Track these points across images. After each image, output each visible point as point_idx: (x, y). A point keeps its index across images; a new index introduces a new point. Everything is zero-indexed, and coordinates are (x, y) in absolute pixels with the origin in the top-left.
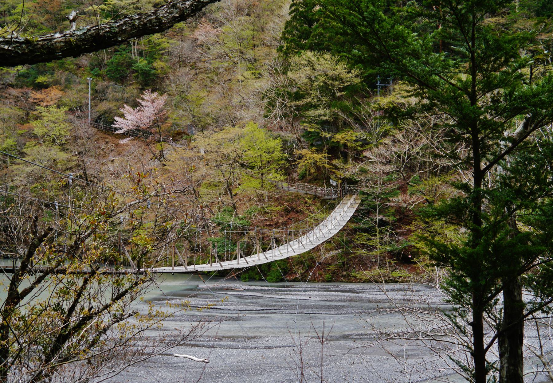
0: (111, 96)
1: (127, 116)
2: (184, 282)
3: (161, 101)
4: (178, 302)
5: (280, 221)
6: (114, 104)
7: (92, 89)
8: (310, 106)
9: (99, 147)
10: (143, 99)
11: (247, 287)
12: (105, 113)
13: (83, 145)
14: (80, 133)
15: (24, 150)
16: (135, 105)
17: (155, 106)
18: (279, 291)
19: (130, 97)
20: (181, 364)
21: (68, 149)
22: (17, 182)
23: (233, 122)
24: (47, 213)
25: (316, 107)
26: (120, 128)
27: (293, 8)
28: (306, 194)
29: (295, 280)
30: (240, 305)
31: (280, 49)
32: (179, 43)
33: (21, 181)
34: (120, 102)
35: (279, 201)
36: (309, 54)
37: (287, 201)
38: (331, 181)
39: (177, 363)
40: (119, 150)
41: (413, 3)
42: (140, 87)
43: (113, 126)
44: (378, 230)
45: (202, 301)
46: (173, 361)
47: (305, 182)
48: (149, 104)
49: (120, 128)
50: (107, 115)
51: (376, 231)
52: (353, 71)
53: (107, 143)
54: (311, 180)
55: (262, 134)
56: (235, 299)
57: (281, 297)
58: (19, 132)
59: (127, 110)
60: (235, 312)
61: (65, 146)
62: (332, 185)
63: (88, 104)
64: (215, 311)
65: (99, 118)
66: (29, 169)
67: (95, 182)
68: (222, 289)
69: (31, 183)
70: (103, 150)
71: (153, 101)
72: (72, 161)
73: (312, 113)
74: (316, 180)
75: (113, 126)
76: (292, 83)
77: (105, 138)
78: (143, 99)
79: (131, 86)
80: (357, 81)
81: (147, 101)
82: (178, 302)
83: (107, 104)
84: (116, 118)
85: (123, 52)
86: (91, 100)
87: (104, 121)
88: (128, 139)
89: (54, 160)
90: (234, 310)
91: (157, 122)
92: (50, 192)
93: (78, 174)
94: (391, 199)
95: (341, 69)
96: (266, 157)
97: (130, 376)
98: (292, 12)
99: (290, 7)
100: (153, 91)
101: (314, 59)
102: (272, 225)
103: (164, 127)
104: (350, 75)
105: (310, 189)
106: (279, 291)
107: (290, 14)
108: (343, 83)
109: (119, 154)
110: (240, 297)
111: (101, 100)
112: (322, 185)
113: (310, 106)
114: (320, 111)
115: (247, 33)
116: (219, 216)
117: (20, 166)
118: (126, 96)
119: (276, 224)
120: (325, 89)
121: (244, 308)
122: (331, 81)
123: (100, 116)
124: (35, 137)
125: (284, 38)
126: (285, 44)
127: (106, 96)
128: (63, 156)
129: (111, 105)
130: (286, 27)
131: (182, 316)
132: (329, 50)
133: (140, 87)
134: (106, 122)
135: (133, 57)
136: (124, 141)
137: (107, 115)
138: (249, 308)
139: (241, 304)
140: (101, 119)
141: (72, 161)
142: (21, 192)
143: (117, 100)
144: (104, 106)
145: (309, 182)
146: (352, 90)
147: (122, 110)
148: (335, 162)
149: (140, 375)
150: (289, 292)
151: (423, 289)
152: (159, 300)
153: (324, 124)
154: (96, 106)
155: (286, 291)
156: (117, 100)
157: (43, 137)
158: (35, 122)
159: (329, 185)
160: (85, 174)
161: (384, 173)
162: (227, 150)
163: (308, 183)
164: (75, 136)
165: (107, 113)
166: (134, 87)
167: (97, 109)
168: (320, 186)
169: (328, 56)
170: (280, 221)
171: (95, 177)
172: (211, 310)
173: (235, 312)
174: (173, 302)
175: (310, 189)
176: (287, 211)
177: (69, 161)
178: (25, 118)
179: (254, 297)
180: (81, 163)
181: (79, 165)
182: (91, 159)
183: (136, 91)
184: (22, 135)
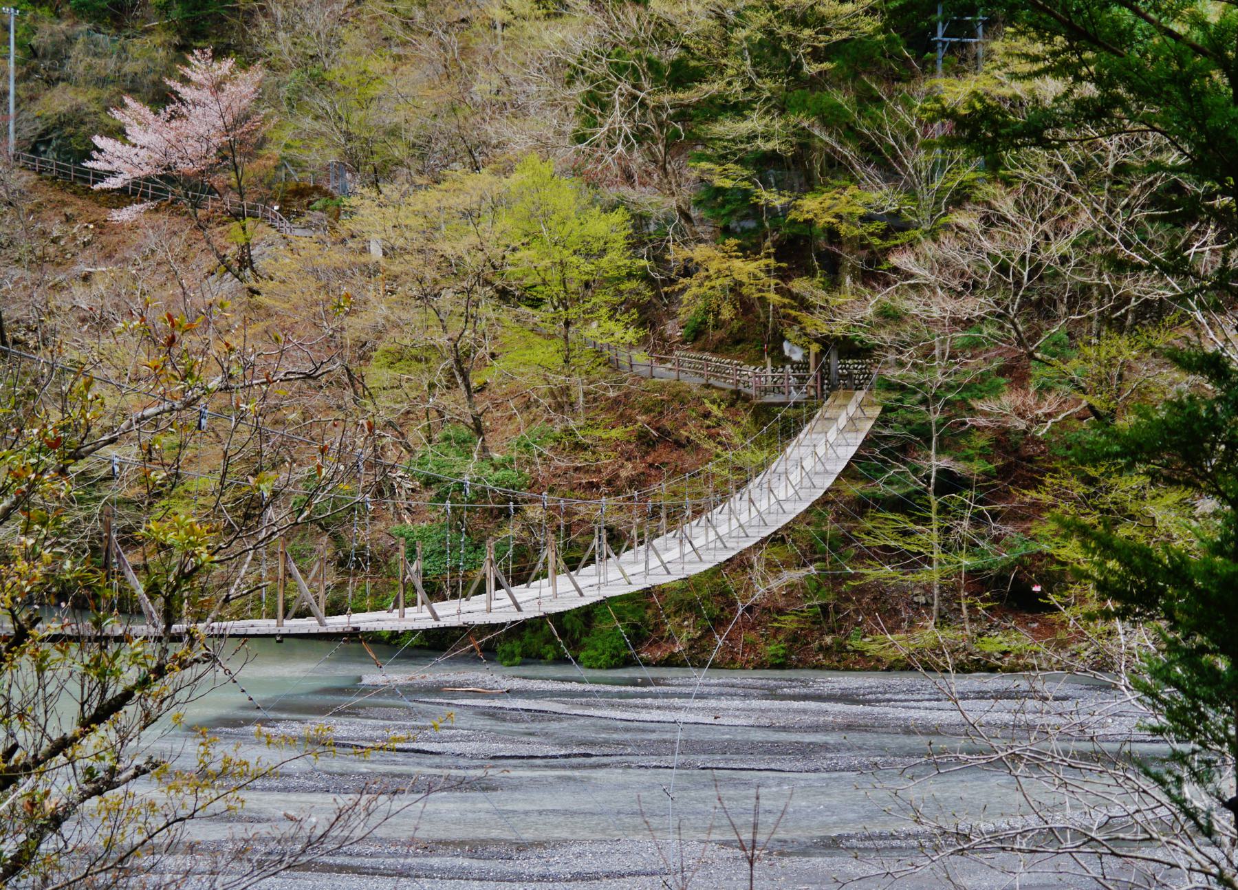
0: (81, 68)
4: (296, 729)
5: (623, 474)
6: (93, 93)
7: (19, 45)
10: (185, 80)
11: (517, 684)
16: (161, 98)
17: (225, 102)
19: (145, 74)
25: (738, 110)
26: (112, 173)
30: (494, 740)
34: (112, 89)
35: (620, 408)
37: (647, 411)
38: (786, 346)
42: (176, 40)
44: (934, 502)
45: (374, 728)
47: (703, 350)
48: (205, 95)
49: (112, 173)
50: (69, 130)
53: (69, 219)
54: (721, 341)
56: (481, 723)
59: (134, 112)
60: (478, 762)
64: (414, 758)
67: (31, 343)
68: (436, 690)
70: (55, 241)
71: (218, 87)
73: (727, 128)
74: (738, 342)
77: (64, 204)
78: (185, 80)
79: (147, 39)
81: (199, 87)
82: (296, 729)
83: (70, 93)
84: (98, 140)
87: (58, 149)
88: (136, 207)
94: (978, 405)
96: (581, 269)
100: (219, 54)
102: (597, 486)
106: (620, 695)
108: (827, 32)
109: (109, 256)
111: (51, 82)
112: (757, 360)
114: (754, 123)
118: (129, 67)
122: (787, 28)
123: (47, 132)
129: (81, 99)
133: (176, 40)
136: (125, 215)
137: (69, 130)
140: (48, 142)
143: (102, 82)
144: (58, 101)
147: (117, 115)
153: (765, 164)
154: (32, 99)
156: (102, 82)
159: (783, 360)
163: (715, 352)
166: (158, 39)
167: (37, 109)
168: (750, 362)
170: (623, 474)
171: (29, 328)
172: (400, 757)
174: (281, 729)
183: (162, 53)
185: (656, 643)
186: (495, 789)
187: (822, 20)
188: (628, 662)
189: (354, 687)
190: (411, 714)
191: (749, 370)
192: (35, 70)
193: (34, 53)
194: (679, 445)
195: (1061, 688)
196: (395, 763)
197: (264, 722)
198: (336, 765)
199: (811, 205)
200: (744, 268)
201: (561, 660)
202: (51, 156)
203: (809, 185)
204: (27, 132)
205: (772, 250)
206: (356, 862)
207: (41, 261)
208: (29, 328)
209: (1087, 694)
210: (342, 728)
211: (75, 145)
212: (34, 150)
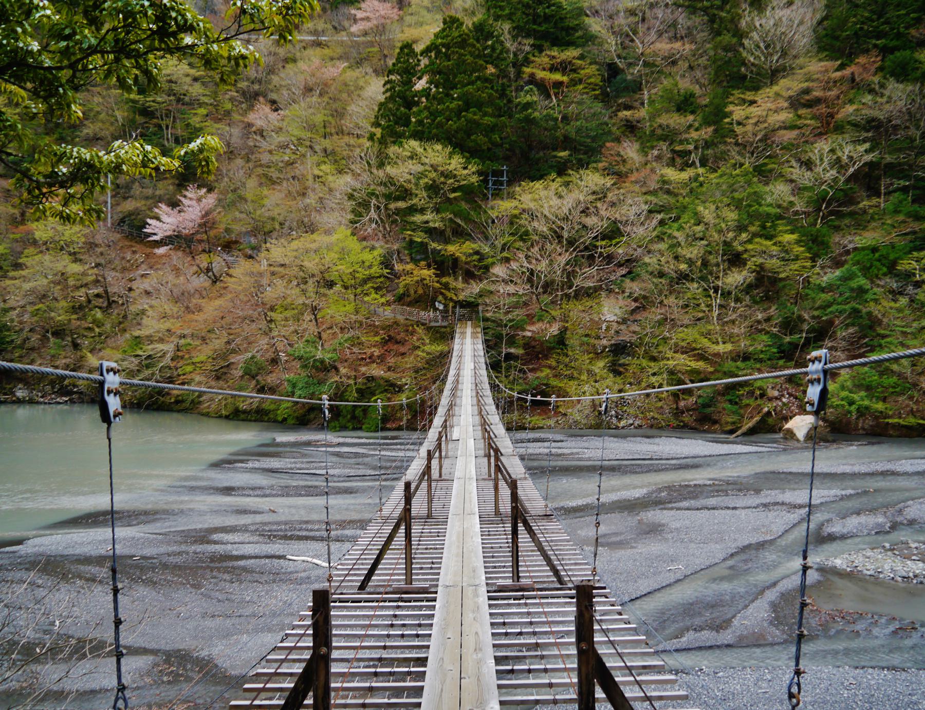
0: (138, 192)
1: (164, 218)
2: (253, 433)
3: (210, 200)
4: (257, 465)
5: (376, 354)
6: (143, 202)
7: (112, 183)
8: (412, 210)
9: (123, 258)
10: (185, 197)
11: (341, 440)
12: (130, 214)
13: (102, 254)
14: (99, 239)
15: (21, 261)
16: (174, 204)
17: (202, 206)
18: (384, 444)
19: (165, 195)
20: (303, 575)
21: (81, 260)
22: (11, 303)
23: (311, 228)
24: (55, 344)
25: (422, 211)
26: (155, 234)
27: (388, 86)
28: (407, 319)
29: (399, 429)
30: (344, 468)
31: (371, 138)
32: (227, 128)
33: (18, 301)
34: (151, 201)
35: (373, 329)
36: (414, 144)
37: (383, 329)
38: (437, 304)
39: (297, 572)
40: (153, 263)
41: (531, 89)
42: (177, 182)
43: (145, 230)
44: (504, 365)
45: (291, 463)
46: (289, 570)
47: (403, 305)
48: (194, 203)
49: (155, 234)
50: (133, 217)
51: (501, 368)
52: (470, 167)
53: (134, 252)
54: (411, 302)
55: (353, 244)
56: (334, 459)
57: (393, 454)
58: (12, 236)
59: (163, 210)
60: (342, 479)
61: (78, 256)
62: (438, 309)
63: (107, 202)
64: (314, 478)
65: (122, 221)
66: (27, 286)
67: (120, 302)
68: (308, 444)
69: (30, 303)
70: (129, 261)
71: (199, 200)
72: (88, 275)
73: (418, 218)
74: (417, 302)
75: (145, 230)
76: (390, 181)
77: (132, 246)
78: (185, 197)
79: (165, 181)
80: (474, 179)
81: (191, 199)
82: (257, 465)
83: (134, 203)
84: (149, 221)
85: (154, 137)
86: (112, 197)
87: (129, 225)
88: (166, 247)
89: (63, 274)
90: (339, 476)
91: (207, 223)
92: (59, 316)
93: (96, 291)
94: (529, 328)
95: (456, 163)
96: (362, 274)
97: (233, 601)
98: (387, 91)
99: (384, 85)
100: (199, 187)
101: (420, 150)
102: (365, 359)
103: (212, 233)
104: (466, 172)
105: (410, 313)
106: (387, 444)
107: (384, 93)
108: (458, 181)
109: (151, 268)
110: (338, 454)
111: (125, 198)
112: (425, 309)
113: (412, 210)
114: (429, 216)
115: (319, 118)
116: (301, 348)
117: (17, 281)
118: (158, 193)
119: (370, 358)
120: (433, 189)
121: (352, 472)
122: (442, 179)
123: (124, 218)
124: (35, 243)
125: (376, 124)
126: (378, 132)
127: (132, 193)
128: (76, 268)
129: (139, 205)
130: (380, 109)
131: (271, 487)
132: (438, 140)
133: (177, 182)
134: (131, 226)
135: (166, 143)
136: (162, 251)
137: (133, 217)
138: (360, 472)
139: (345, 466)
140: (124, 222)
141: (88, 275)
142: (18, 316)
143: (147, 198)
144: (129, 206)
145: (409, 304)
146: (469, 193)
147: (156, 210)
148: (444, 280)
149: (248, 598)
150: (399, 447)
151: (565, 439)
152: (229, 462)
153: (432, 232)
154: (118, 204)
155: (396, 444)
156: (147, 198)
157: (45, 243)
158: (36, 223)
159: (436, 309)
160: (106, 292)
161: (509, 294)
162: (311, 265)
163: (408, 306)
164: (91, 243)
165: (133, 214)
166: (170, 182)
167: (119, 209)
168: (423, 310)
169: (439, 147)
170: (376, 354)
171: (119, 296)
172: (307, 477)
173: (342, 479)
174: (250, 465)
175: (410, 313)
176: (385, 342)
177: (84, 274)
178: (19, 219)
179: (356, 455)
180: (100, 278)
181: (97, 281)
182: (113, 274)
183: (171, 187)
184: (16, 241)
185: (393, 422)
186: (356, 492)
187: (455, 176)
188: (383, 429)
189: (274, 444)
190: (304, 456)
191: (422, 313)
192: (119, 193)
193: (118, 186)
194: (397, 342)
195: (558, 437)
196: (306, 480)
197: (242, 461)
198: (283, 482)
199: (451, 248)
200: (426, 273)
201: (354, 429)
202: (126, 228)
203: (447, 241)
204: (115, 217)
205: (745, 256)
206: (312, 534)
207: (124, 269)
208: (119, 296)
209: (570, 439)
210: (274, 463)
211: (136, 223)
212: (119, 224)
